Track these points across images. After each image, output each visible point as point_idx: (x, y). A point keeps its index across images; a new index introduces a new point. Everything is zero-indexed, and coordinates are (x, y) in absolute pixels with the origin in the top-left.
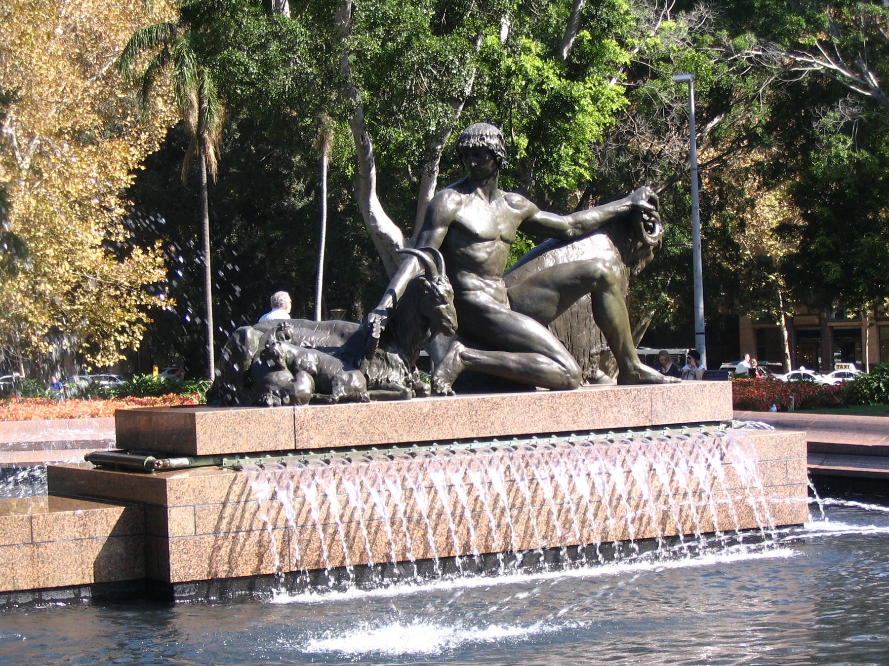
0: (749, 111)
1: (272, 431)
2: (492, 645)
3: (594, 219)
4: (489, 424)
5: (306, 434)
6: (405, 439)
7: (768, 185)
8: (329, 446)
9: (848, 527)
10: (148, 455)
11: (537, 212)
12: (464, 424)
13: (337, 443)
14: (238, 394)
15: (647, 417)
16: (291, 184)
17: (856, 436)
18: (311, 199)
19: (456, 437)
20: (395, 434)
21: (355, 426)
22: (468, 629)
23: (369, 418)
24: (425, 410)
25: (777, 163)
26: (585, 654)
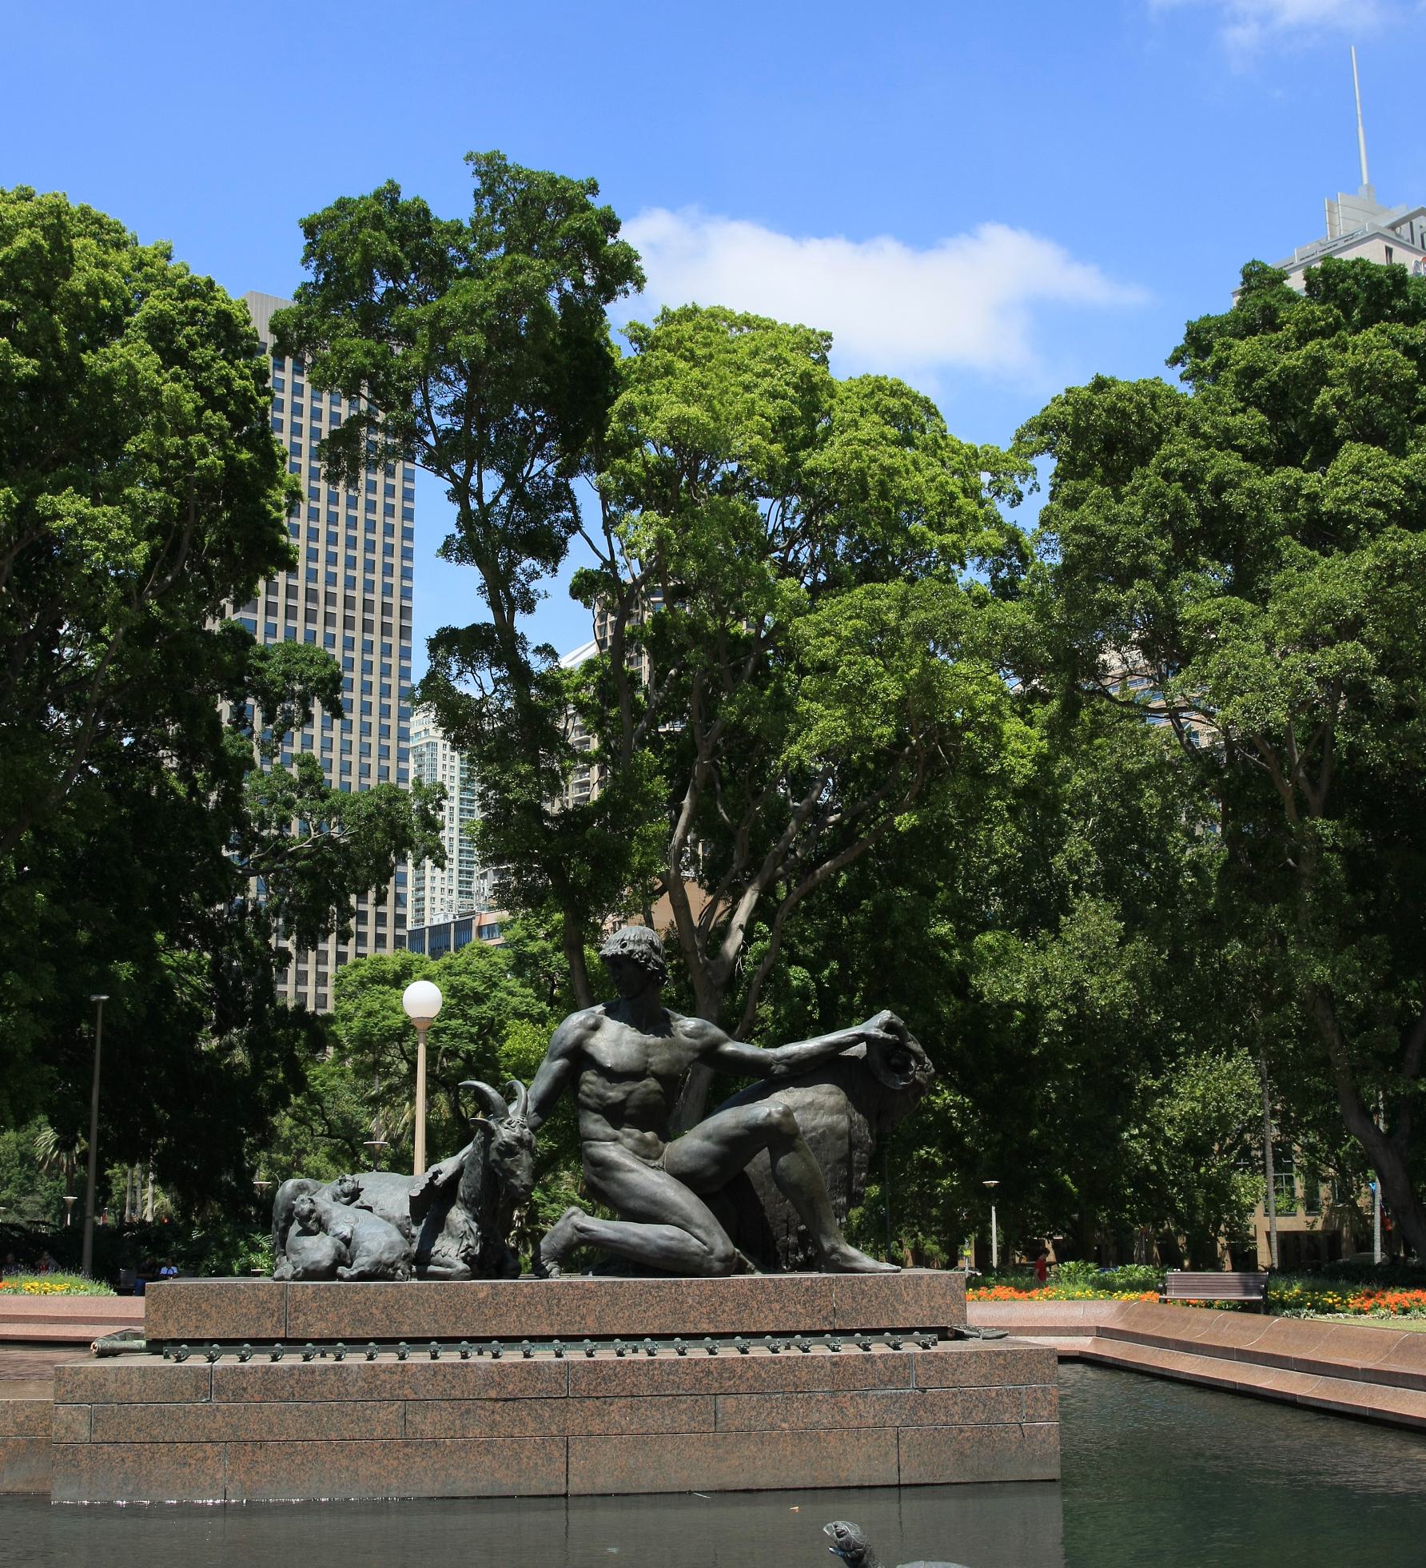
0: (532, 982)
1: (254, 1312)
2: (1005, 1237)
3: (664, 1061)
4: (578, 1318)
5: (302, 1318)
6: (449, 1333)
7: (936, 1197)
8: (335, 1336)
9: (1103, 1310)
10: (227, 859)
11: (726, 1041)
12: (539, 1317)
13: (347, 1333)
14: (242, 894)
15: (825, 1318)
16: (1019, 1006)
17: (634, 1240)
18: (826, 972)
19: (526, 1334)
20: (434, 1326)
21: (375, 1311)
22: (1269, 473)
23: (397, 1302)
24: (481, 1295)
25: (1232, 1206)
26: (675, 841)
